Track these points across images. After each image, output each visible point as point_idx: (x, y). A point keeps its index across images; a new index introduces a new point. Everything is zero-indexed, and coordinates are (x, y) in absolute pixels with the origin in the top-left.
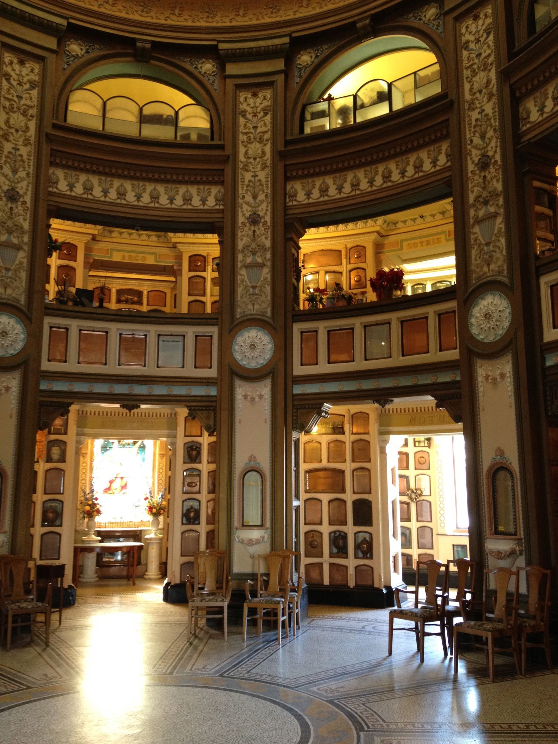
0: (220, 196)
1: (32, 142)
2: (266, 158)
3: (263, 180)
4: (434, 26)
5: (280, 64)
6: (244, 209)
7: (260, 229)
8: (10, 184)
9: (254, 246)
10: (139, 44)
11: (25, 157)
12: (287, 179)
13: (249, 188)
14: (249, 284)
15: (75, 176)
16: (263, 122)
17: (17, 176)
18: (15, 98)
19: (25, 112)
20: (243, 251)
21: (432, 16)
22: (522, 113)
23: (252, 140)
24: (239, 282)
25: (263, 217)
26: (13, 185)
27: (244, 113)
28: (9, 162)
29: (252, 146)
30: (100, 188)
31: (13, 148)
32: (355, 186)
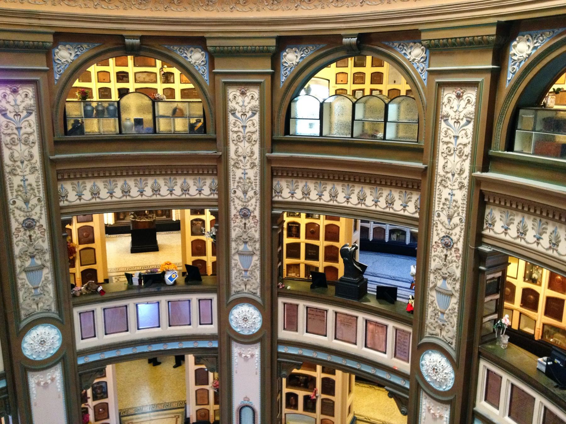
0: (214, 186)
1: (38, 168)
3: (460, 202)
6: (236, 203)
7: (250, 222)
8: (25, 214)
9: (444, 270)
11: (34, 185)
12: (273, 176)
13: (240, 184)
14: (242, 268)
15: (82, 184)
16: (251, 122)
20: (235, 241)
21: (417, 56)
22: (487, 217)
23: (242, 139)
24: (233, 265)
25: (253, 212)
26: (28, 214)
28: (20, 195)
29: (242, 144)
30: (106, 189)
31: (22, 180)
32: (390, 203)
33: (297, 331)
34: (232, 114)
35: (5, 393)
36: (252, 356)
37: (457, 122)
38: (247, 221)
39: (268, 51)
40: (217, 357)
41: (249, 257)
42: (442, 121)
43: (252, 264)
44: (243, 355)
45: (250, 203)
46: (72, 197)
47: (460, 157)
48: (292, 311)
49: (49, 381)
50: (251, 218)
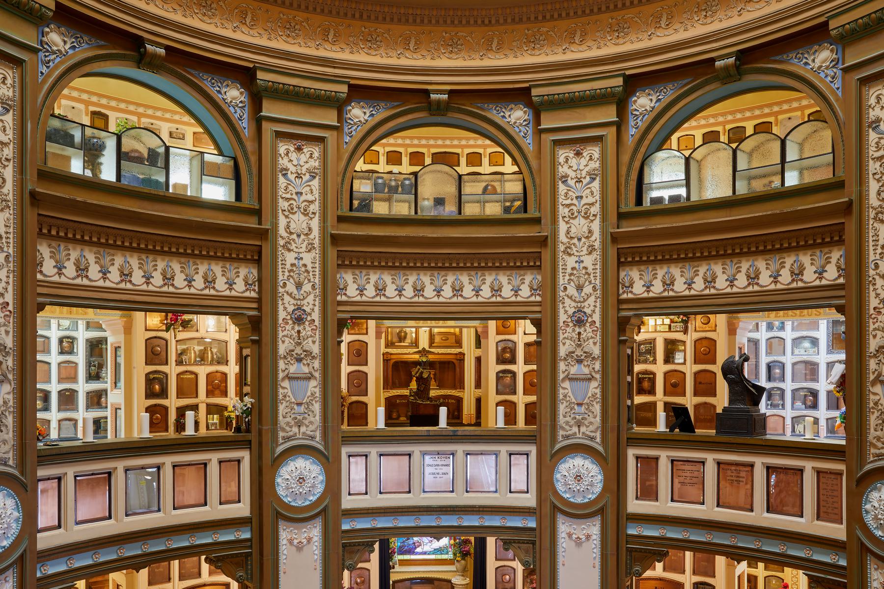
2: (593, 238)
4: (826, 76)
5: (609, 114)
7: (587, 331)
8: (295, 302)
10: (433, 96)
11: (309, 268)
12: (620, 264)
13: (572, 277)
16: (308, 188)
17: (583, 294)
18: (294, 196)
19: (305, 210)
23: (576, 214)
24: (561, 397)
26: (299, 302)
27: (285, 172)
29: (575, 222)
31: (296, 258)
33: (657, 500)
34: (563, 182)
35: (247, 548)
36: (588, 537)
39: (613, 95)
40: (533, 543)
42: (871, 130)
43: (590, 395)
44: (574, 536)
45: (586, 304)
46: (639, 289)
47: (586, 218)
48: (649, 465)
49: (305, 541)
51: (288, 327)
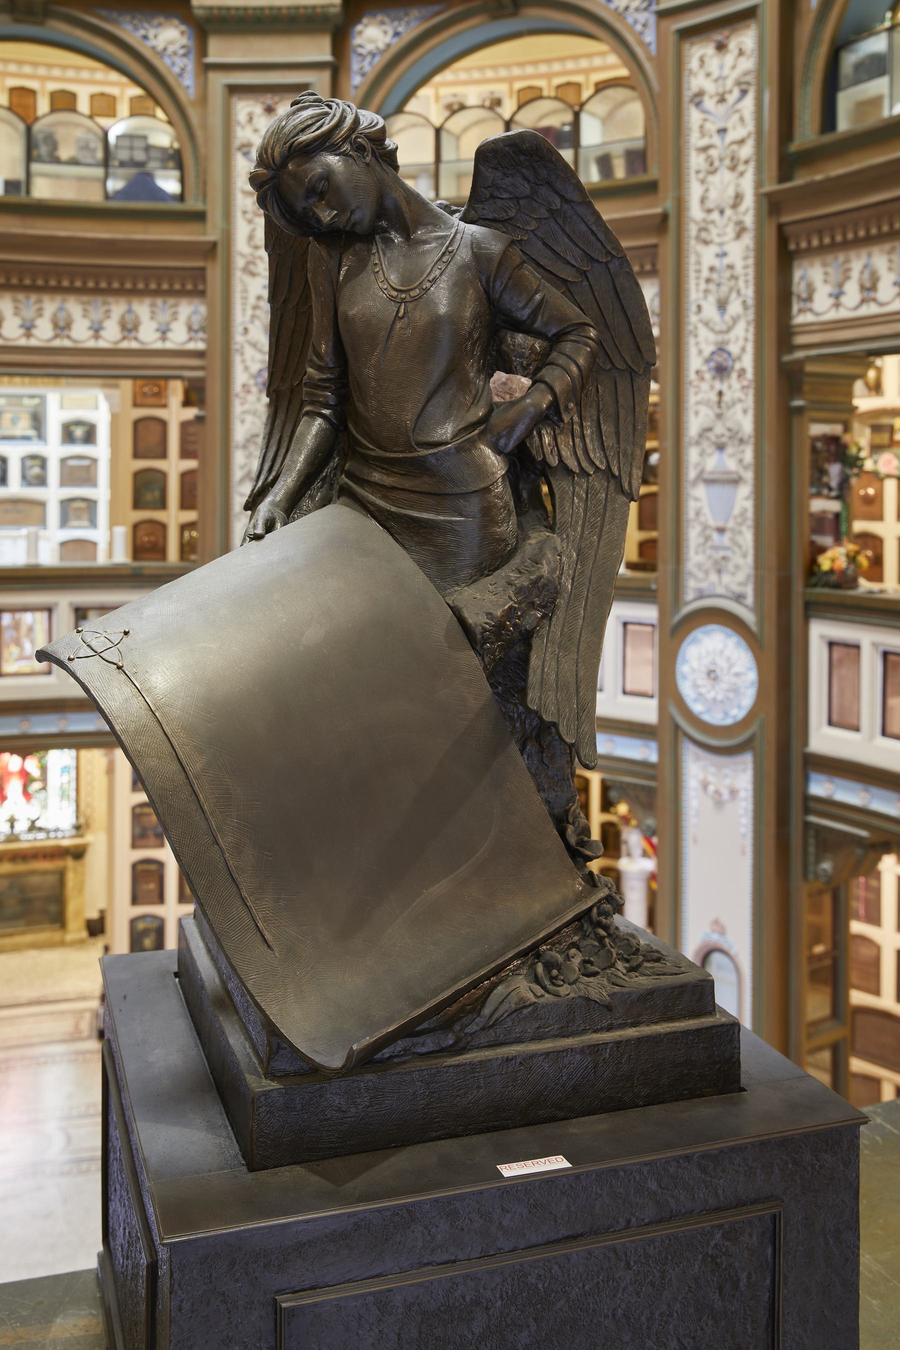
3: (739, 264)
5: (319, 49)
6: (701, 339)
9: (719, 429)
13: (258, 312)
20: (245, 447)
25: (739, 358)
29: (714, 179)
36: (733, 793)
37: (722, 100)
38: (724, 387)
41: (726, 490)
47: (733, 168)
50: (734, 375)
51: (705, 386)
